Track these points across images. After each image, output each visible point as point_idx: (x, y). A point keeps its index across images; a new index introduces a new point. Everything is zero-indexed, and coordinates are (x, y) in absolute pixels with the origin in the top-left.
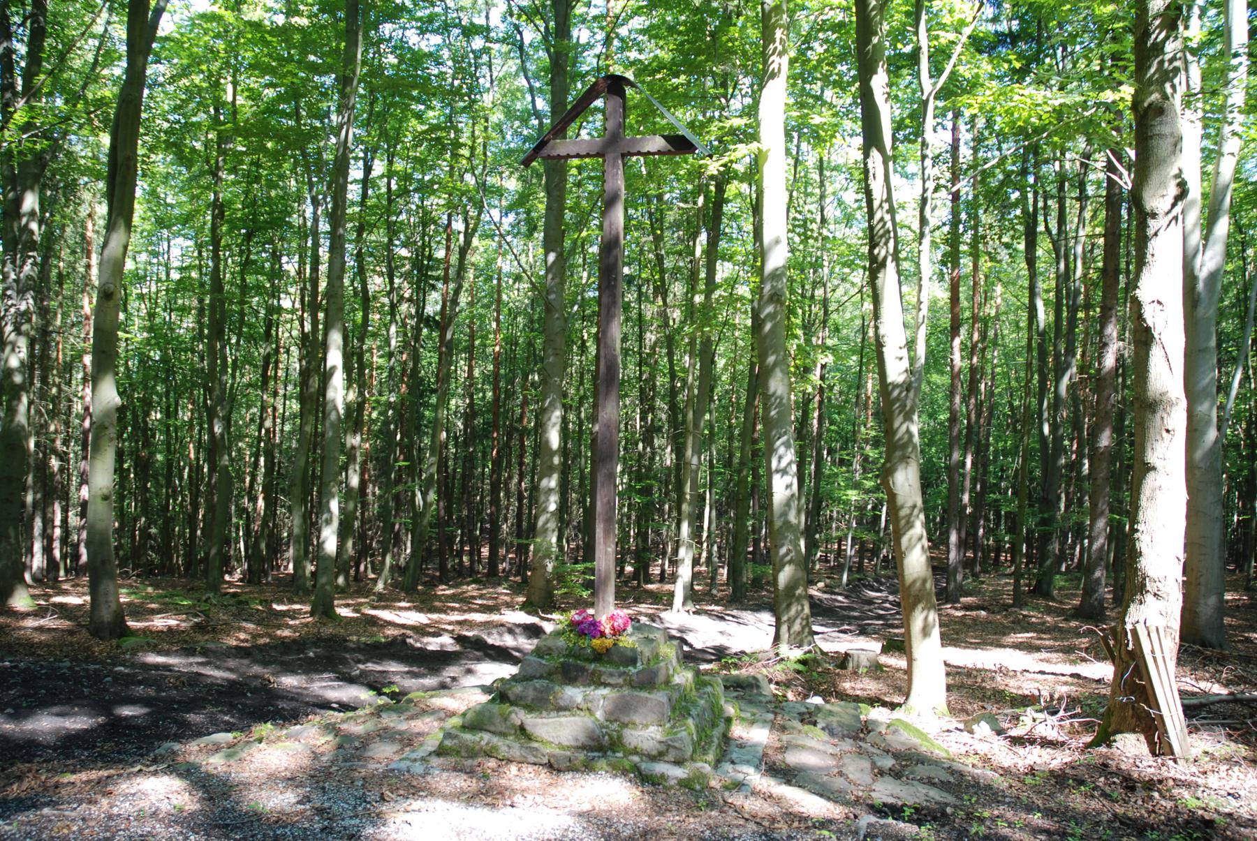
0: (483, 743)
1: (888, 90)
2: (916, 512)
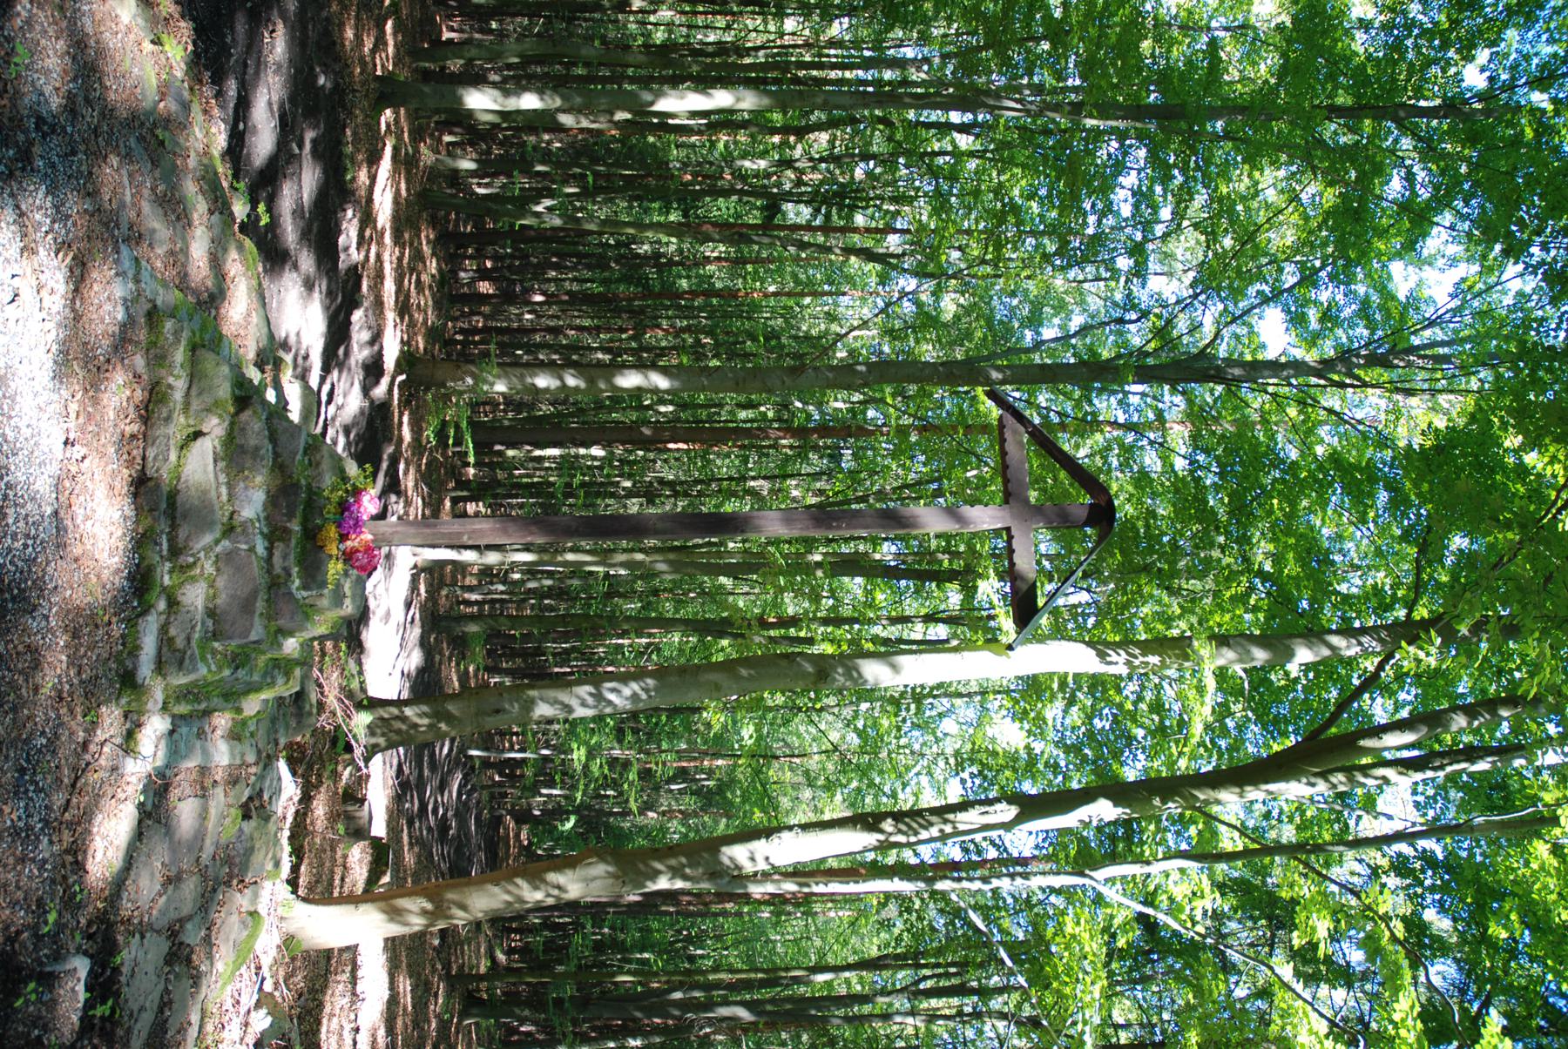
0: (171, 380)
1: (1095, 823)
2: (556, 892)
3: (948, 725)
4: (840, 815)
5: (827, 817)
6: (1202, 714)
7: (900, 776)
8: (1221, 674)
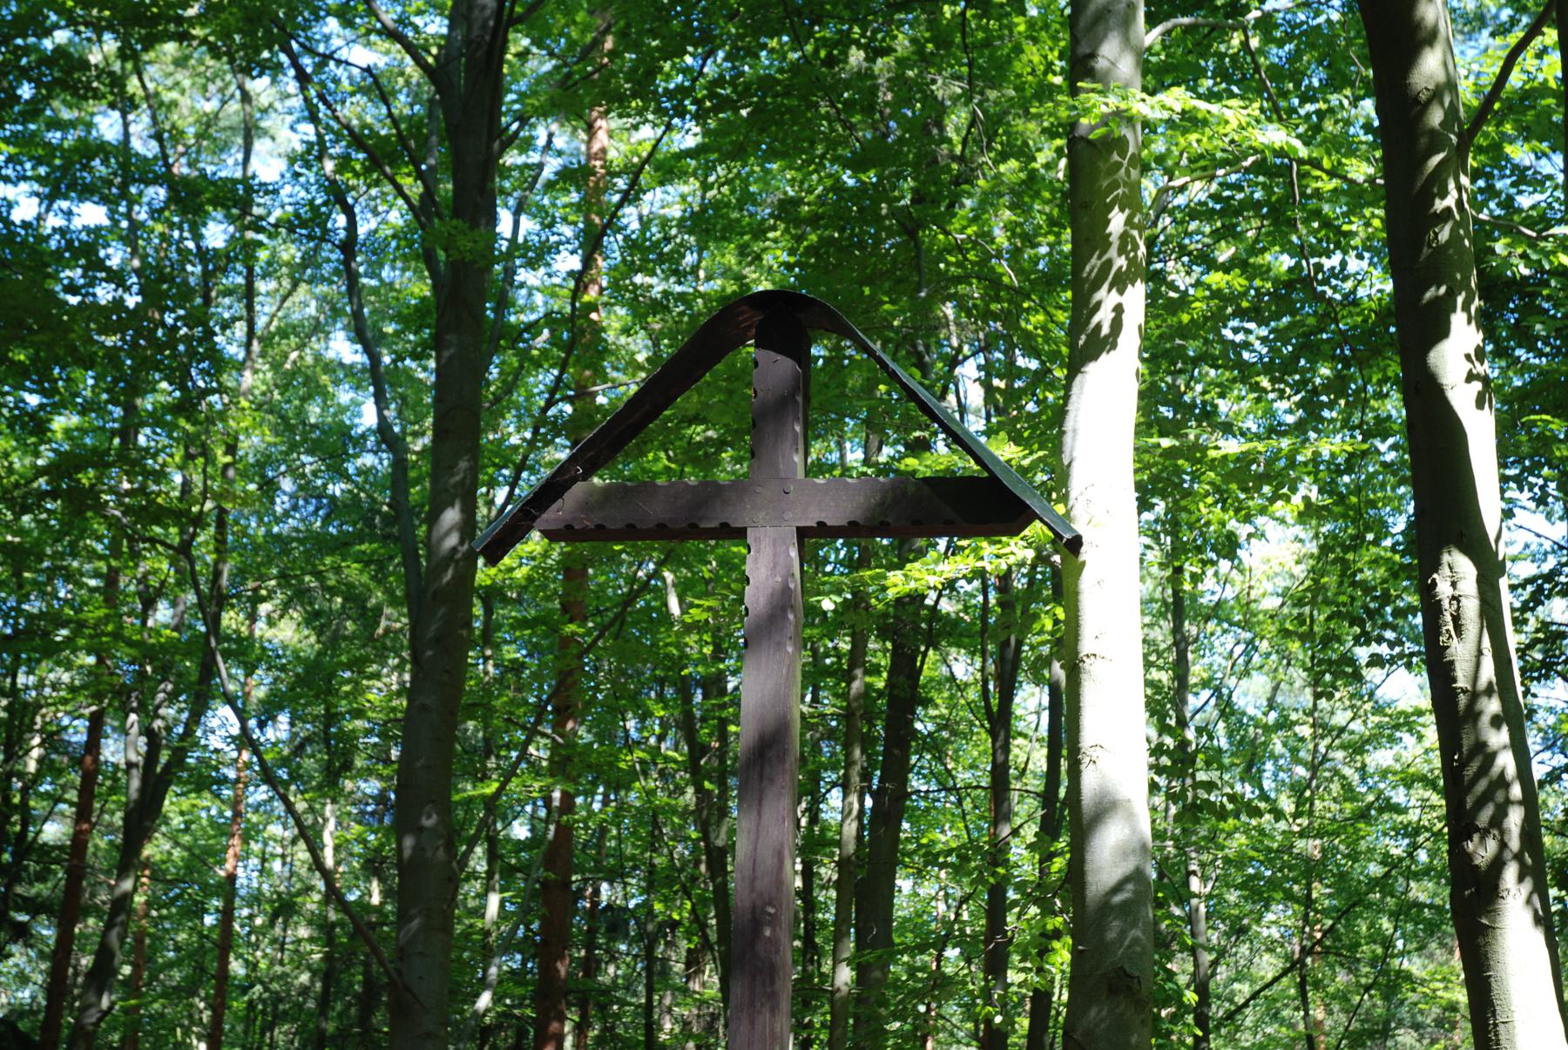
3: (1250, 695)
4: (1457, 962)
5: (1461, 996)
6: (1237, 119)
7: (1363, 815)
8: (1157, 76)
